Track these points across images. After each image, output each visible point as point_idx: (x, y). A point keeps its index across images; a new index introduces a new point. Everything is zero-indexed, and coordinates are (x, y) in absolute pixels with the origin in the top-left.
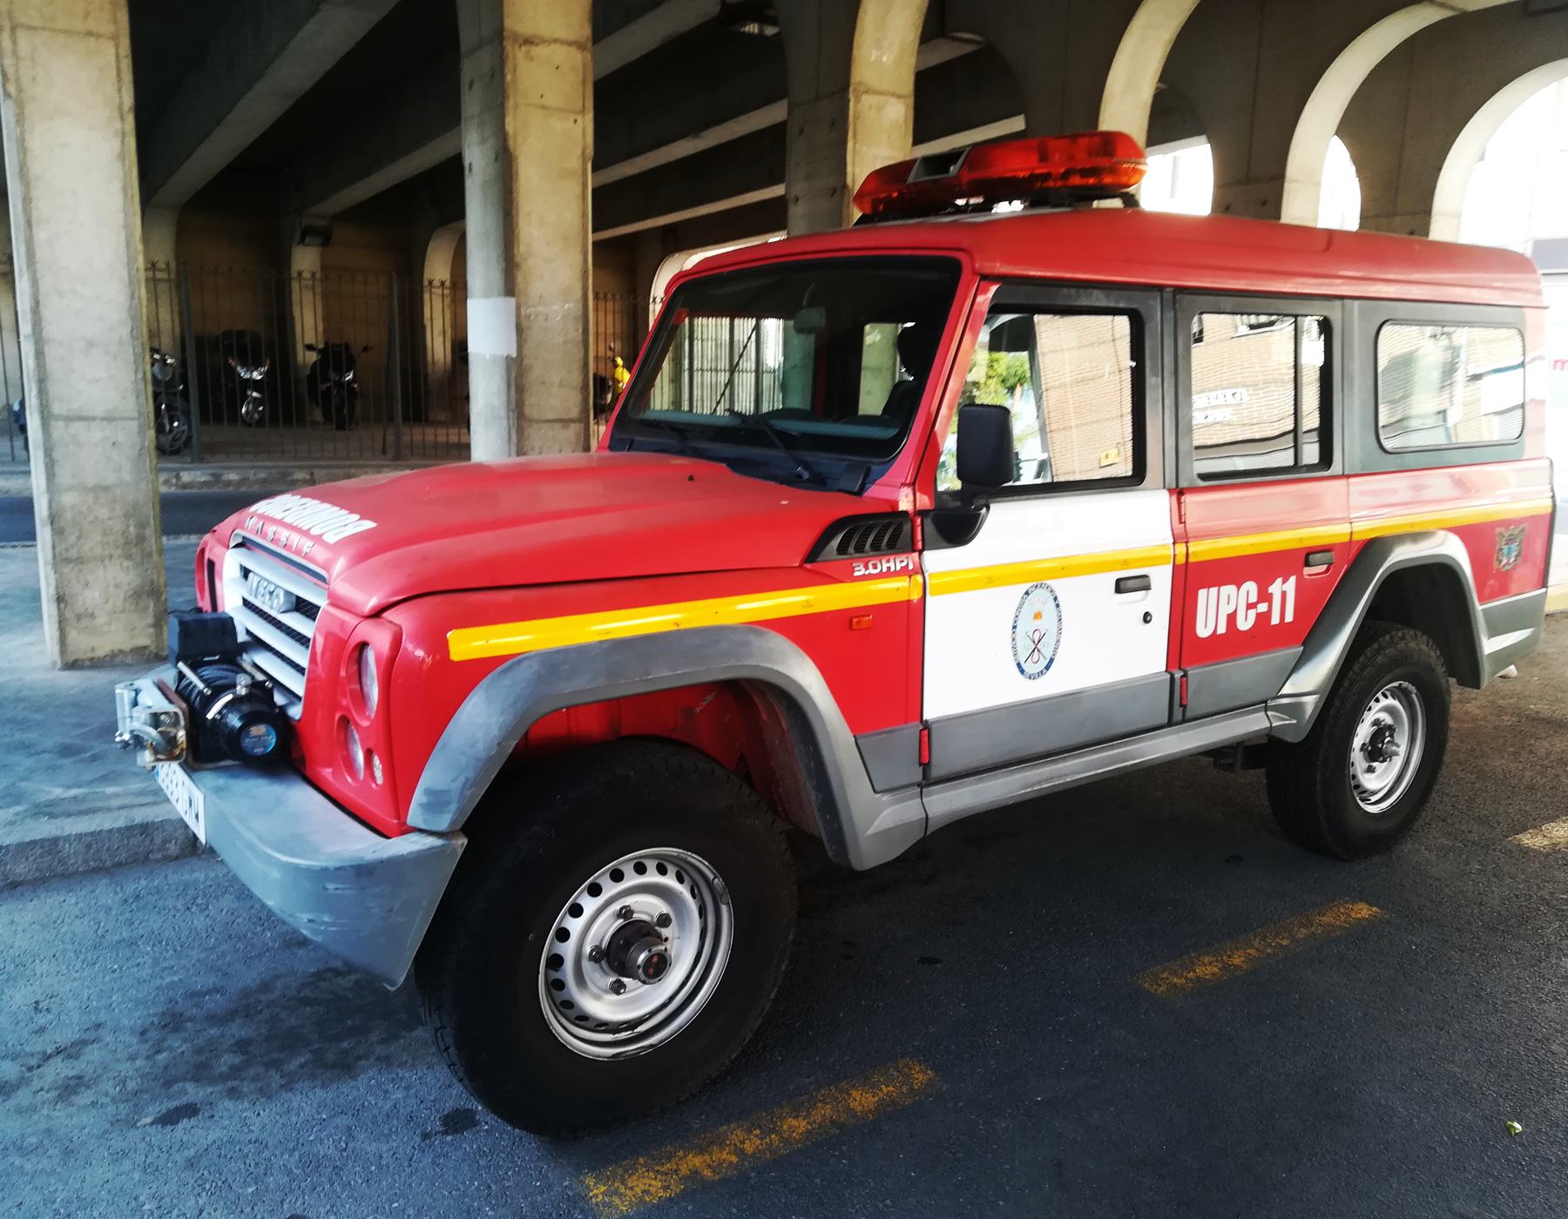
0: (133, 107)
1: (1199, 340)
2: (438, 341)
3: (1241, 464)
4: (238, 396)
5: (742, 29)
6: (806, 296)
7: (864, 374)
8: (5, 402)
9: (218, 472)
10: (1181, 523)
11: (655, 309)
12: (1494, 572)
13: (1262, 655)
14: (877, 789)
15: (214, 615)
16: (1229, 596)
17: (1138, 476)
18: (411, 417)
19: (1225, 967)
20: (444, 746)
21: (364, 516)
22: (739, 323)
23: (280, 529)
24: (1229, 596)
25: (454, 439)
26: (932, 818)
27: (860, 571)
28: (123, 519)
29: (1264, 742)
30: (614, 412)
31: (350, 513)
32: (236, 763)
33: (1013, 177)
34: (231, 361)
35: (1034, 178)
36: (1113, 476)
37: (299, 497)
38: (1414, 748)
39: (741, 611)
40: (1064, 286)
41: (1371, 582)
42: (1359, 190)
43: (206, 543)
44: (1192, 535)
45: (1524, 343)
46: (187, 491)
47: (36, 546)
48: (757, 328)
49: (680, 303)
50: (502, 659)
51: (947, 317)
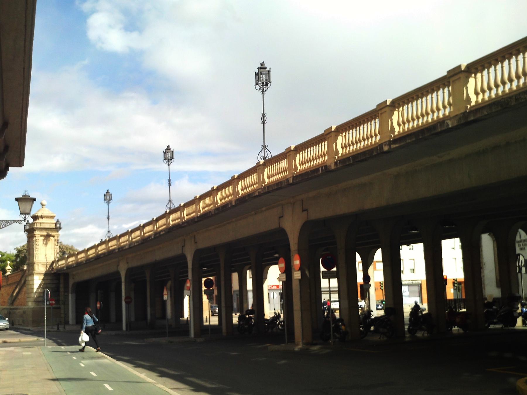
0: (292, 257)
1: (401, 249)
2: (173, 373)
3: (335, 292)
4: (284, 295)
5: (373, 154)
6: (50, 296)
7: (404, 298)
8: (169, 199)
9: (518, 48)
10: (303, 211)
11: (158, 368)
12: (7, 319)
13: (234, 305)
14: (360, 270)
15: (273, 291)
16: (410, 259)
17: (39, 265)
18: (286, 341)
19: (524, 266)
20: (404, 291)
21: (80, 365)
22: (296, 277)
23: (258, 191)
24: (410, 259)
25: (462, 307)
26: (454, 297)
27: (168, 291)
28: (62, 227)
29: (524, 268)
30: (146, 377)
31: (53, 342)
32: (165, 288)
33: (59, 344)
34: (426, 335)
35: (131, 235)
36: (301, 322)
37: (8, 171)
38: (515, 70)
39: (367, 293)
40: (276, 189)
41: (47, 314)
42: (34, 38)
43: (446, 123)
44: (406, 282)
45: (279, 225)
46: (306, 166)
47: (411, 272)
48: (405, 285)
49: (24, 307)
50: (169, 388)
51: (32, 45)
